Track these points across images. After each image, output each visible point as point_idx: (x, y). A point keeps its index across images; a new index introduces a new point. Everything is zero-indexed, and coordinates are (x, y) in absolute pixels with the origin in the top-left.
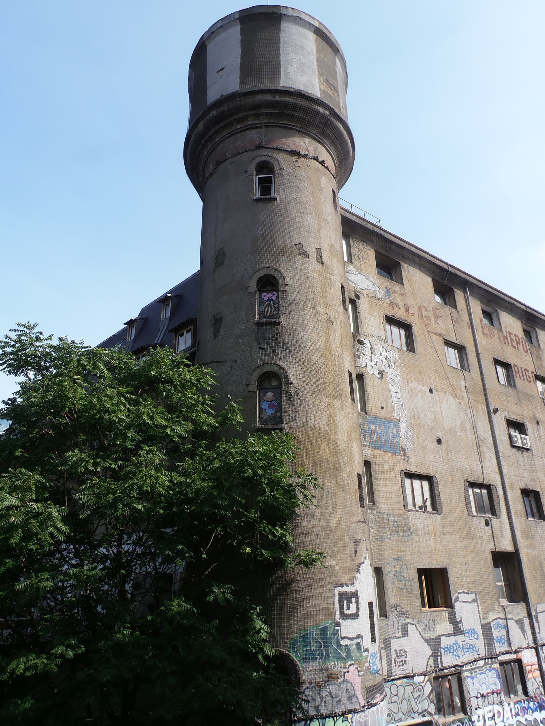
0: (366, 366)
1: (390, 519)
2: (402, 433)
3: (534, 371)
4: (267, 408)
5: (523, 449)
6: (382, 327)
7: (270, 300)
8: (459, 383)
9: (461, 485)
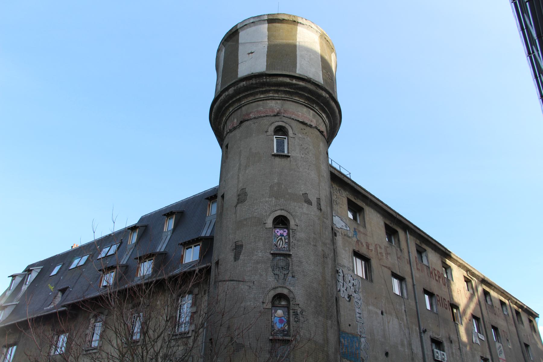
2: (362, 346)
6: (351, 260)
7: (282, 235)
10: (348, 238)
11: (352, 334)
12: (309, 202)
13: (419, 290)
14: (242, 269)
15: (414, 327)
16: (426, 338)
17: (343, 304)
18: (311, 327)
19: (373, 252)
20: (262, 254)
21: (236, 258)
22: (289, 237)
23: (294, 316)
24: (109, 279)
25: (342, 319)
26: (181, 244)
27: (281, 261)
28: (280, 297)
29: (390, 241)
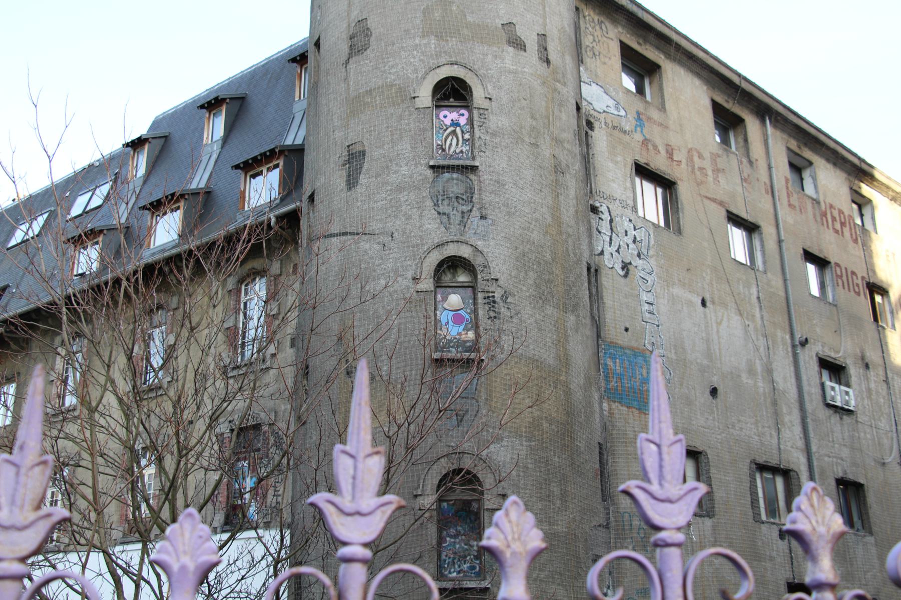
0: (602, 253)
1: (634, 523)
3: (866, 276)
4: (450, 322)
5: (844, 411)
6: (628, 184)
7: (455, 124)
8: (749, 291)
9: (745, 468)
10: (621, 135)
11: (632, 349)
12: (519, 45)
13: (793, 254)
14: (366, 207)
15: (779, 333)
16: (810, 369)
17: (610, 282)
18: (530, 332)
19: (683, 165)
20: (411, 168)
21: (351, 183)
22: (472, 127)
23: (487, 307)
24: (88, 260)
25: (609, 316)
26: (237, 167)
27: (454, 184)
28: (453, 264)
29: (725, 141)
